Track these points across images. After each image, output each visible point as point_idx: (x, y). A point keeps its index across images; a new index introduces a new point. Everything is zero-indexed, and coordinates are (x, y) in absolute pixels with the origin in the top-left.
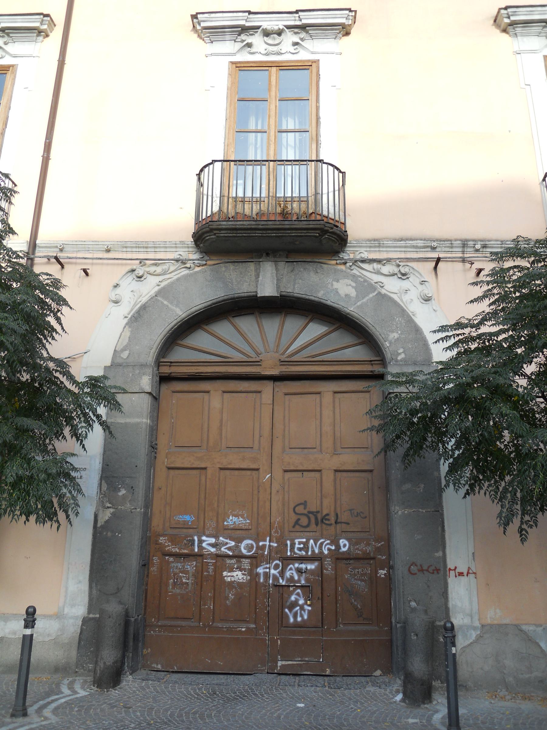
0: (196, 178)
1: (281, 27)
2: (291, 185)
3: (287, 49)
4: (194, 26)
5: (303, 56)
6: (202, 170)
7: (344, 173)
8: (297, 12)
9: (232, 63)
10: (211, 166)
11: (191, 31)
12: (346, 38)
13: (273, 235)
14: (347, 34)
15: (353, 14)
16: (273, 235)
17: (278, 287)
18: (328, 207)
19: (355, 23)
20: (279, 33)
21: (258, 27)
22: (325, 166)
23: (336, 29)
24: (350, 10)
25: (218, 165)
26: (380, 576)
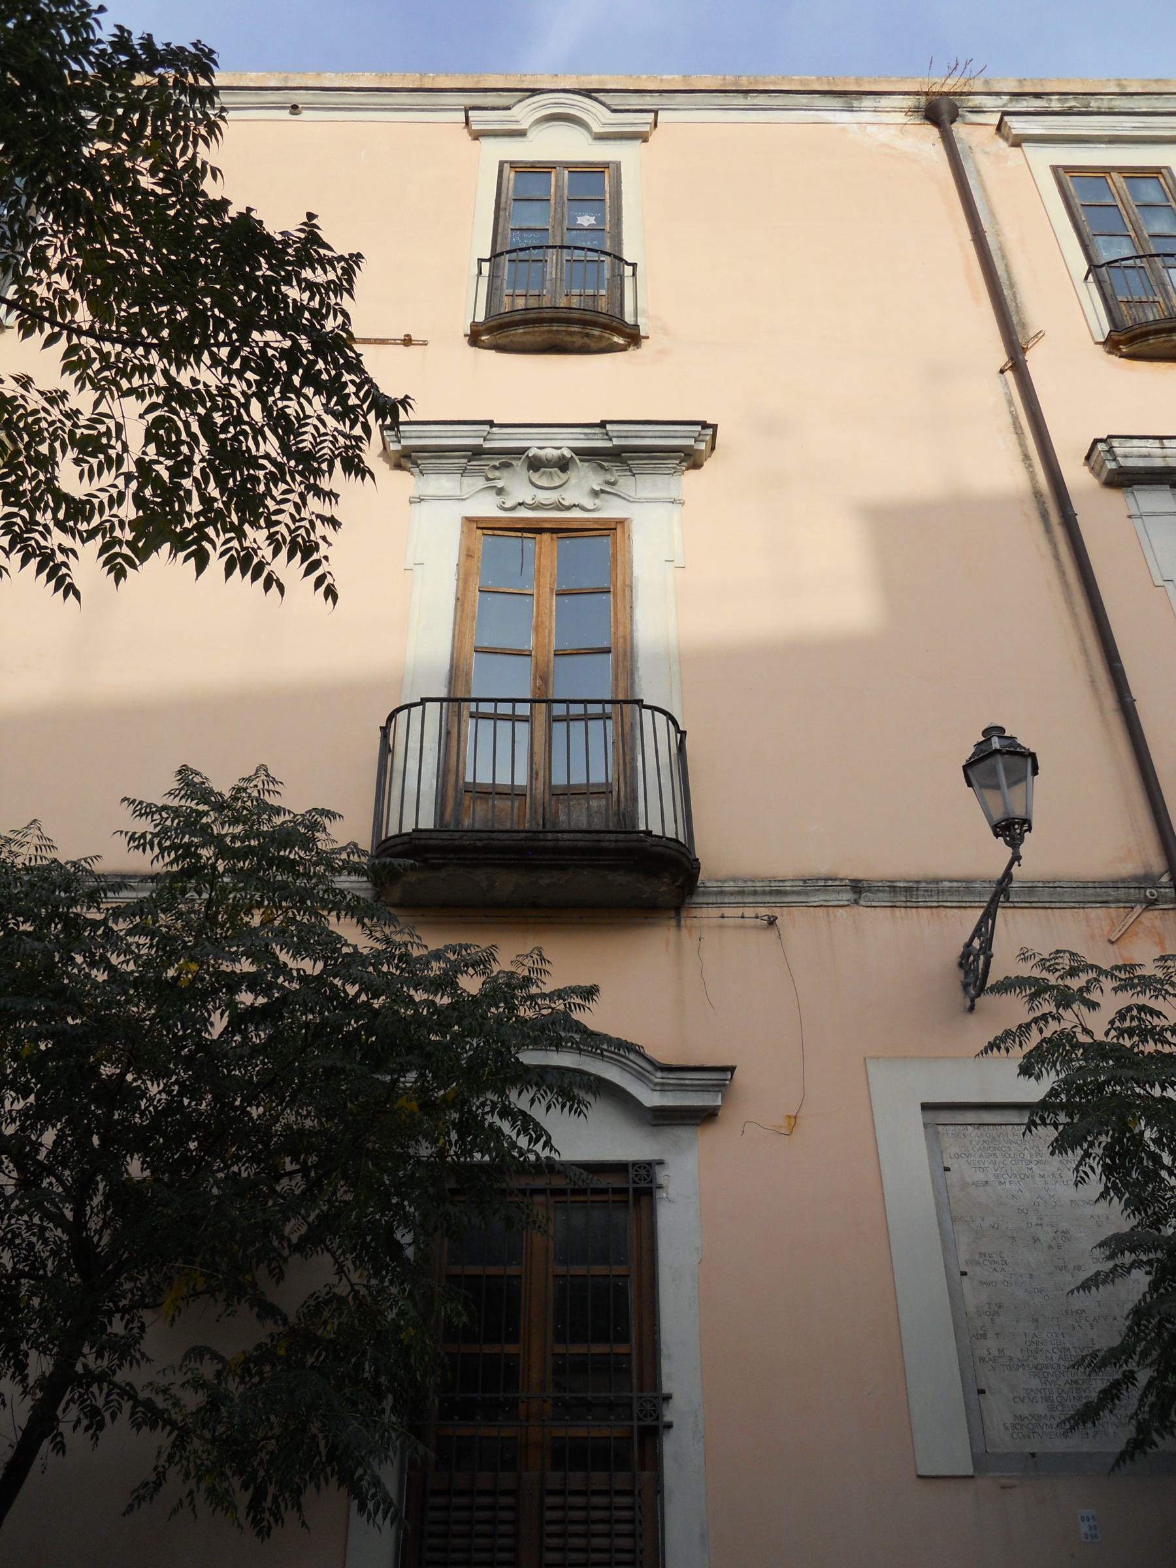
0: (379, 734)
1: (568, 454)
2: (584, 759)
3: (579, 495)
4: (385, 448)
5: (611, 510)
6: (392, 716)
7: (683, 733)
8: (603, 424)
9: (469, 520)
10: (416, 711)
11: (379, 456)
12: (693, 472)
13: (551, 857)
14: (697, 466)
15: (710, 431)
16: (551, 857)
17: (449, 692)
18: (655, 816)
19: (713, 448)
20: (563, 465)
21: (522, 451)
22: (647, 713)
23: (675, 458)
24: (704, 425)
25: (433, 709)
26: (467, 1043)
